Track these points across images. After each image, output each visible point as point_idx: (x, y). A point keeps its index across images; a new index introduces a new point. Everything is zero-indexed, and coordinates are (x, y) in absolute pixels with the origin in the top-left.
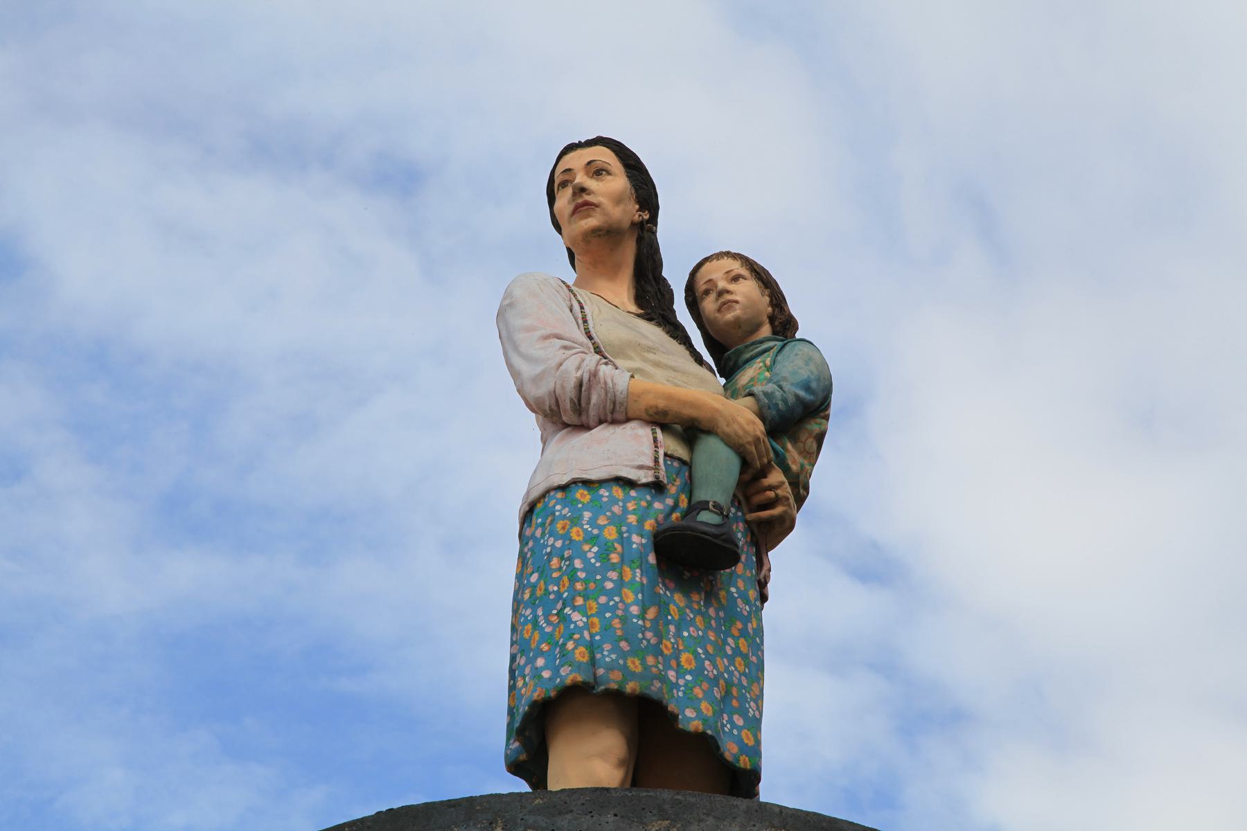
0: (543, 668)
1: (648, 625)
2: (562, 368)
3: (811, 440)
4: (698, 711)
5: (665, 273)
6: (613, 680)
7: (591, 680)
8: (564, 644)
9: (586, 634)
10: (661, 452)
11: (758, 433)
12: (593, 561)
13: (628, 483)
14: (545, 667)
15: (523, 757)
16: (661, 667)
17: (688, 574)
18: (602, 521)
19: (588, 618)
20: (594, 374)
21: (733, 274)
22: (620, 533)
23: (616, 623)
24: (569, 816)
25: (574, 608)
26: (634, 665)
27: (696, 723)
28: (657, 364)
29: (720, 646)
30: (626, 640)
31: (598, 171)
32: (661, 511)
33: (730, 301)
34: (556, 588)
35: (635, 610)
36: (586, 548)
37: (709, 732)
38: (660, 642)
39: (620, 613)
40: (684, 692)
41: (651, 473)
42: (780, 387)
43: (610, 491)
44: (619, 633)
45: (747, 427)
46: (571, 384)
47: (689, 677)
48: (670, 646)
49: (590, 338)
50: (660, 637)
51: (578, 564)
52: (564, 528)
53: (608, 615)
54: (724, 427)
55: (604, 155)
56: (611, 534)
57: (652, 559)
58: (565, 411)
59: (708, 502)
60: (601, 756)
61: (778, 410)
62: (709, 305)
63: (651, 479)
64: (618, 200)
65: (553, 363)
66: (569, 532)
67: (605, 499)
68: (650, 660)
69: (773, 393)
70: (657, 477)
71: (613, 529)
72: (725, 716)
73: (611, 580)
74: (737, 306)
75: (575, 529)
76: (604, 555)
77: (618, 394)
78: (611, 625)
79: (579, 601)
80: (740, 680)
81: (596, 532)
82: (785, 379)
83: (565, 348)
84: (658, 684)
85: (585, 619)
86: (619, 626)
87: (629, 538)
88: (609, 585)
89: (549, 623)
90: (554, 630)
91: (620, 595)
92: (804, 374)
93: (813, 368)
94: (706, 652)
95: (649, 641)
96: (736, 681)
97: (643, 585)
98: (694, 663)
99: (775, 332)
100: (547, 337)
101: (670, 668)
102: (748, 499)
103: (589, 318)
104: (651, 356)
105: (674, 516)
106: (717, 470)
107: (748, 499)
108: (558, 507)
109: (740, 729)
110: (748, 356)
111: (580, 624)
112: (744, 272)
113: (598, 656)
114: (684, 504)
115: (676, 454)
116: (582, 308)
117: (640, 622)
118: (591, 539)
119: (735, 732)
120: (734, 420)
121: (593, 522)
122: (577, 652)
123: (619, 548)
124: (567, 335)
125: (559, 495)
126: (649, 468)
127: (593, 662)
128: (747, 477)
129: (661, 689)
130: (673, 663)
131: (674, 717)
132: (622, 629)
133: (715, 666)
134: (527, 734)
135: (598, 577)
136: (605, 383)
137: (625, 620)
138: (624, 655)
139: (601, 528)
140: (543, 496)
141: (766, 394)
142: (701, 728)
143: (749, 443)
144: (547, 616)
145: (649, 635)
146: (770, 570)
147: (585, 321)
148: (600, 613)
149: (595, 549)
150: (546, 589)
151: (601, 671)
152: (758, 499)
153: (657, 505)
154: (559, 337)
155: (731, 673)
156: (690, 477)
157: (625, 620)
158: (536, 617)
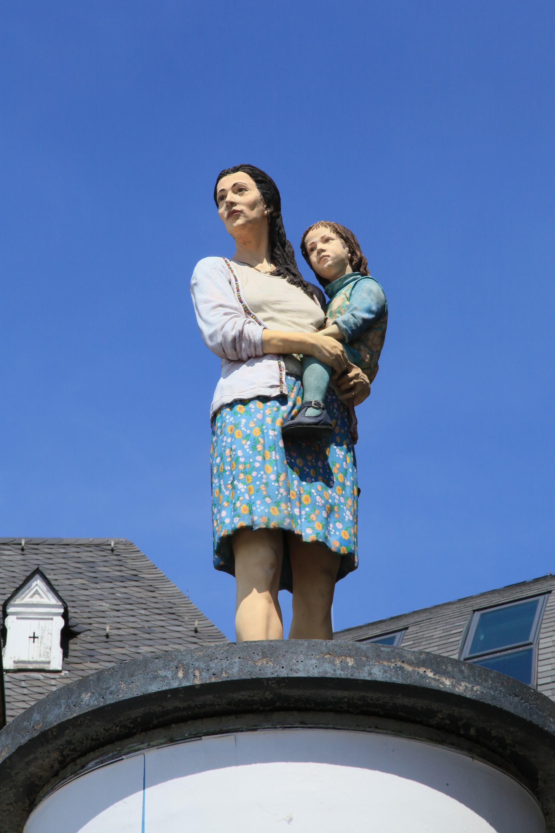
0: (225, 517)
1: (281, 484)
2: (224, 329)
3: (376, 338)
4: (313, 528)
5: (222, 382)
6: (260, 522)
7: (251, 524)
8: (235, 504)
9: (247, 497)
11: (339, 353)
12: (248, 450)
13: (264, 399)
15: (222, 563)
16: (289, 509)
17: (304, 444)
18: (252, 425)
19: (247, 485)
20: (241, 333)
22: (262, 431)
24: (216, 661)
25: (239, 481)
26: (275, 511)
28: (281, 311)
30: (269, 497)
31: (239, 189)
32: (285, 412)
33: (324, 256)
35: (273, 477)
36: (244, 442)
37: (320, 540)
38: (289, 493)
39: (264, 481)
40: (306, 519)
43: (255, 405)
44: (265, 493)
47: (307, 509)
48: (295, 493)
49: (241, 302)
50: (288, 490)
51: (240, 453)
52: (231, 430)
53: (258, 483)
56: (256, 433)
57: (281, 444)
58: (229, 355)
59: (311, 402)
62: (314, 257)
64: (252, 206)
65: (218, 326)
66: (233, 433)
67: (253, 410)
68: (283, 506)
69: (348, 320)
70: (281, 392)
71: (258, 429)
72: (331, 525)
73: (259, 462)
74: (329, 259)
75: (237, 431)
76: (253, 447)
77: (256, 342)
78: (260, 489)
79: (242, 476)
80: (339, 500)
81: (248, 432)
82: (355, 309)
83: (226, 314)
84: (288, 521)
85: (245, 487)
86: (264, 489)
87: (267, 432)
88: (257, 465)
91: (263, 470)
93: (373, 297)
94: (317, 491)
95: (282, 494)
96: (336, 501)
97: (276, 460)
98: (310, 500)
99: (354, 270)
100: (215, 307)
101: (296, 507)
102: (339, 387)
103: (240, 288)
106: (316, 376)
107: (339, 387)
108: (228, 417)
109: (340, 530)
111: (243, 490)
112: (333, 235)
113: (254, 508)
114: (299, 404)
115: (293, 372)
116: (236, 280)
117: (276, 484)
118: (247, 437)
121: (247, 426)
122: (242, 508)
123: (261, 440)
124: (227, 304)
125: (228, 410)
126: (278, 386)
127: (251, 512)
128: (336, 377)
129: (290, 524)
130: (297, 504)
132: (266, 491)
133: (322, 497)
134: (222, 552)
135: (251, 460)
137: (267, 485)
138: (268, 506)
139: (251, 429)
141: (344, 322)
142: (315, 539)
144: (226, 485)
145: (282, 490)
146: (357, 423)
147: (238, 291)
148: (254, 482)
149: (249, 443)
150: (224, 469)
151: (255, 518)
152: (344, 387)
153: (284, 408)
154: (221, 306)
155: (333, 498)
157: (267, 485)
158: (220, 485)
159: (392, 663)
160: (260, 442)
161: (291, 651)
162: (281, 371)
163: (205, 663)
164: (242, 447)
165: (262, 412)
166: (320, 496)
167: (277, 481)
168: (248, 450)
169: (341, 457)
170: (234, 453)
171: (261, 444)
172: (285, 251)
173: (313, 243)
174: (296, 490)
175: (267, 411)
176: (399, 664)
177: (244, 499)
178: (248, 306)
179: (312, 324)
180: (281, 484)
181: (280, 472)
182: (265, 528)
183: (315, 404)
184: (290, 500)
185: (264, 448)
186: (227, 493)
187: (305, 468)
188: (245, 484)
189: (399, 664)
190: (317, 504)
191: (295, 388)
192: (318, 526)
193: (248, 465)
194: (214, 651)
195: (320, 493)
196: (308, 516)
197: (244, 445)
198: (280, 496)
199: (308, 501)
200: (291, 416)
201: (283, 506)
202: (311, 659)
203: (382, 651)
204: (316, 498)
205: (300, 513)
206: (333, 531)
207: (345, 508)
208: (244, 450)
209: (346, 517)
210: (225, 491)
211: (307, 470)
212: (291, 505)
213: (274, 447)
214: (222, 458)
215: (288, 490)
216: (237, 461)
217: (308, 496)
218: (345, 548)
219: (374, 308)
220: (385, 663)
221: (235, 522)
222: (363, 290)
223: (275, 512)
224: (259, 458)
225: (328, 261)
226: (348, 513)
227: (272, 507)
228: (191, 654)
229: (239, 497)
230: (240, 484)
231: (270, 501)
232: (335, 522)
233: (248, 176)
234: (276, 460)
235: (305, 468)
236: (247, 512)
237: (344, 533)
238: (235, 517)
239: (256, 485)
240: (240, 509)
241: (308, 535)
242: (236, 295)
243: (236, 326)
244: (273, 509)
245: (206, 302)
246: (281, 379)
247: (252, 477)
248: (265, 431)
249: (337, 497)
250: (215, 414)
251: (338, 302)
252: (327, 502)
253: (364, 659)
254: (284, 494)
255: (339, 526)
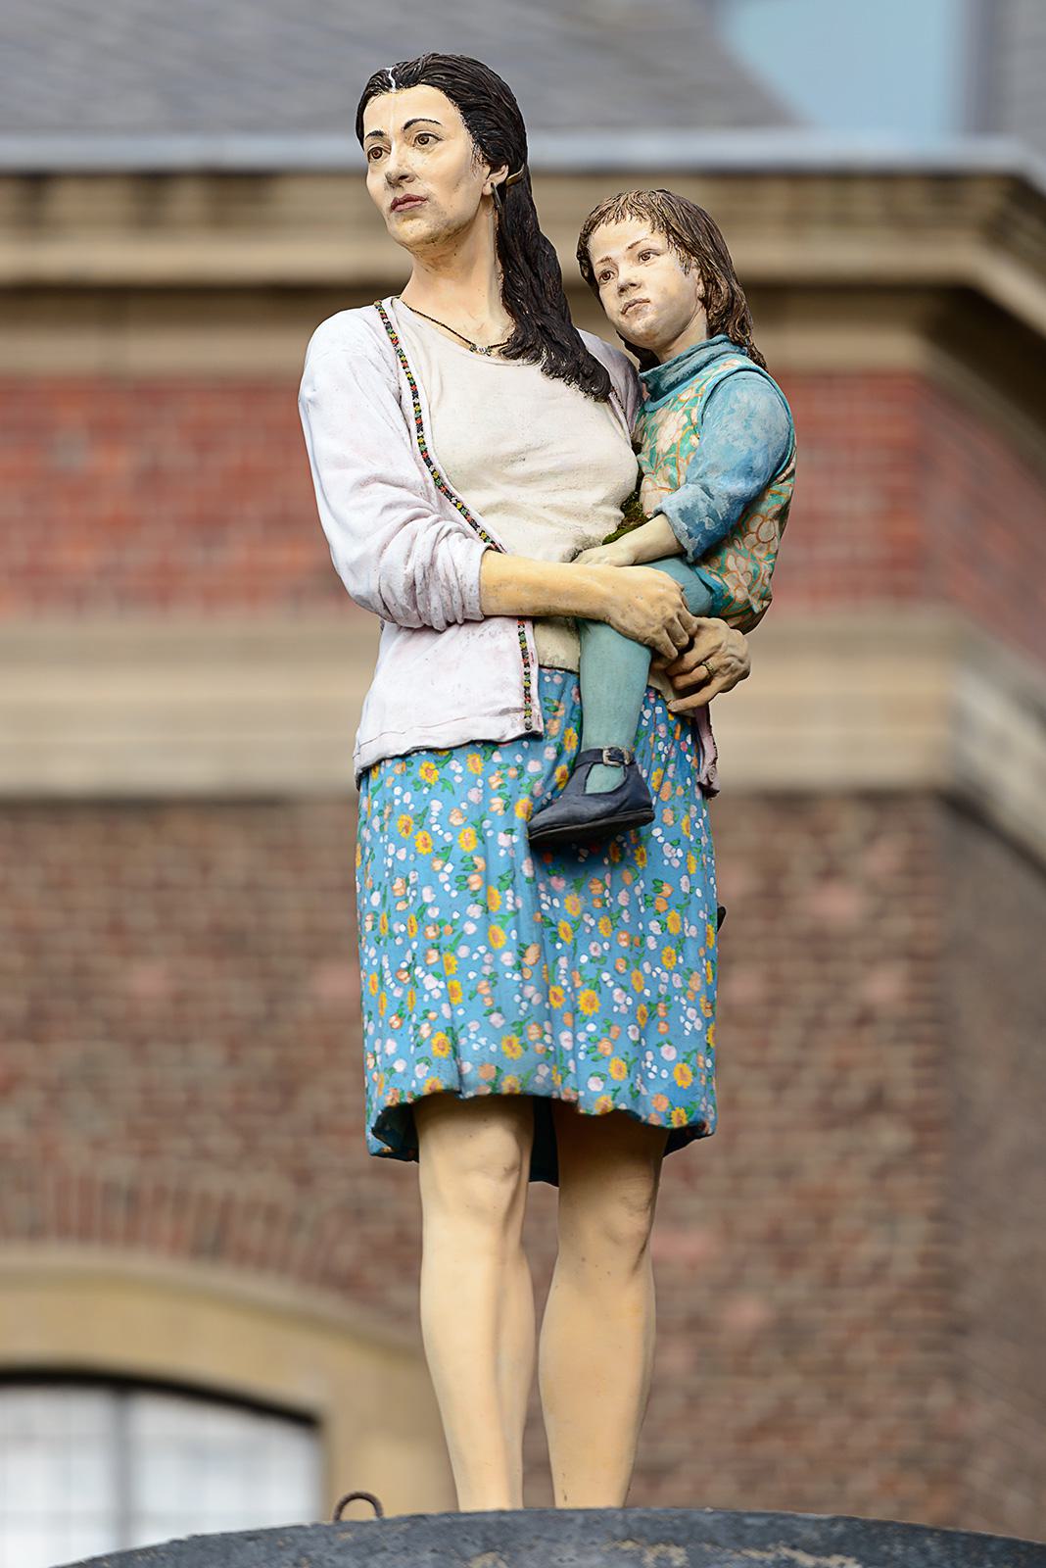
4: (604, 1077)
7: (456, 1087)
10: (534, 670)
12: (447, 887)
13: (491, 745)
14: (398, 1055)
16: (548, 1039)
21: (639, 249)
23: (484, 987)
24: (382, 1556)
27: (602, 1100)
28: (529, 479)
29: (637, 951)
32: (538, 777)
34: (403, 928)
35: (508, 958)
36: (438, 865)
37: (623, 1107)
39: (487, 970)
41: (520, 716)
42: (706, 490)
44: (488, 1002)
45: (650, 611)
46: (400, 586)
47: (591, 1028)
49: (429, 463)
53: (472, 975)
54: (617, 617)
55: (428, 103)
59: (601, 751)
60: (483, 1168)
61: (705, 532)
63: (520, 731)
64: (454, 182)
72: (649, 1056)
73: (473, 920)
75: (420, 835)
76: (461, 882)
78: (477, 992)
80: (670, 984)
81: (448, 837)
84: (544, 1071)
85: (442, 985)
86: (487, 991)
87: (495, 837)
89: (398, 982)
90: (404, 995)
92: (743, 449)
93: (756, 430)
98: (597, 1003)
99: (712, 332)
100: (364, 483)
104: (520, 469)
105: (558, 773)
106: (614, 674)
108: (398, 791)
110: (670, 379)
112: (658, 241)
113: (463, 1041)
114: (571, 749)
116: (415, 394)
117: (517, 977)
118: (445, 852)
119: (664, 1074)
120: (631, 605)
122: (434, 1042)
123: (479, 862)
125: (398, 768)
126: (517, 710)
129: (549, 1078)
130: (568, 1019)
131: (570, 1107)
132: (492, 997)
135: (456, 916)
136: (447, 580)
137: (493, 979)
139: (454, 830)
140: (379, 763)
142: (610, 1107)
143: (657, 632)
145: (530, 991)
147: (420, 427)
148: (462, 972)
149: (449, 868)
152: (682, 681)
153: (533, 767)
156: (579, 694)
157: (493, 979)
159: (769, 1551)
160: (476, 867)
161: (546, 1535)
162: (527, 665)
163: (358, 1558)
164: (431, 879)
165: (480, 783)
166: (622, 987)
167: (519, 967)
168: (447, 887)
169: (676, 863)
170: (414, 893)
171: (479, 873)
172: (537, 275)
173: (608, 259)
174: (564, 983)
175: (492, 779)
176: (786, 1552)
177: (440, 1016)
178: (444, 476)
179: (604, 502)
180: (527, 974)
181: (527, 942)
182: (490, 1095)
183: (610, 758)
184: (550, 1015)
185: (486, 882)
186: (398, 993)
187: (586, 917)
188: (439, 976)
189: (786, 1552)
190: (616, 1009)
191: (562, 706)
192: (616, 1069)
193: (448, 927)
194: (377, 1532)
195: (622, 980)
196: (593, 1043)
197: (441, 990)
198: (524, 1005)
199: (592, 1006)
200: (551, 786)
201: (533, 1032)
202: (589, 1553)
203: (747, 1527)
204: (611, 995)
205: (575, 1039)
206: (655, 1069)
207: (684, 1001)
208: (437, 888)
209: (687, 1024)
210: (392, 986)
211: (592, 922)
212: (553, 1027)
213: (510, 880)
214: (384, 898)
215: (545, 991)
216: (421, 916)
217: (593, 993)
218: (682, 1111)
219: (759, 462)
220: (755, 1554)
221: (419, 1076)
222: (732, 411)
223: (514, 1050)
224: (475, 911)
225: (646, 313)
226: (691, 1012)
227: (506, 1038)
228: (326, 1536)
229: (428, 1011)
230: (430, 976)
231: (502, 1022)
232: (660, 1045)
233: (441, 95)
234: (516, 912)
235: (586, 917)
236: (446, 1054)
237: (681, 1070)
238: (418, 1062)
239: (468, 980)
240: (430, 1045)
241: (593, 1096)
242: (416, 441)
243: (415, 554)
244: (510, 1043)
245: (341, 464)
246: (527, 688)
247: (458, 958)
248: (489, 834)
249: (665, 975)
250: (365, 773)
251: (670, 425)
252: (639, 998)
253: (707, 1547)
254: (536, 1000)
255: (669, 1053)
